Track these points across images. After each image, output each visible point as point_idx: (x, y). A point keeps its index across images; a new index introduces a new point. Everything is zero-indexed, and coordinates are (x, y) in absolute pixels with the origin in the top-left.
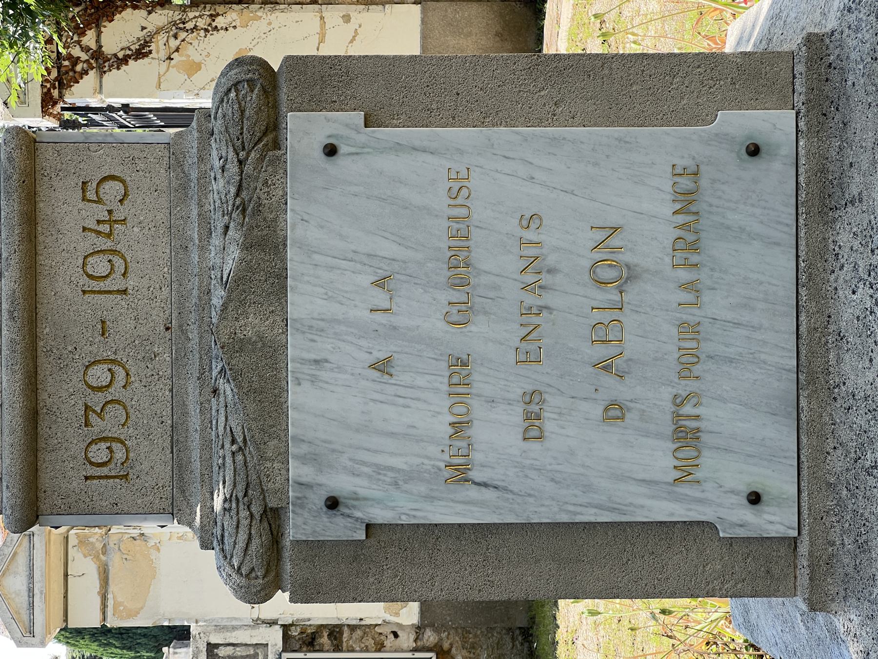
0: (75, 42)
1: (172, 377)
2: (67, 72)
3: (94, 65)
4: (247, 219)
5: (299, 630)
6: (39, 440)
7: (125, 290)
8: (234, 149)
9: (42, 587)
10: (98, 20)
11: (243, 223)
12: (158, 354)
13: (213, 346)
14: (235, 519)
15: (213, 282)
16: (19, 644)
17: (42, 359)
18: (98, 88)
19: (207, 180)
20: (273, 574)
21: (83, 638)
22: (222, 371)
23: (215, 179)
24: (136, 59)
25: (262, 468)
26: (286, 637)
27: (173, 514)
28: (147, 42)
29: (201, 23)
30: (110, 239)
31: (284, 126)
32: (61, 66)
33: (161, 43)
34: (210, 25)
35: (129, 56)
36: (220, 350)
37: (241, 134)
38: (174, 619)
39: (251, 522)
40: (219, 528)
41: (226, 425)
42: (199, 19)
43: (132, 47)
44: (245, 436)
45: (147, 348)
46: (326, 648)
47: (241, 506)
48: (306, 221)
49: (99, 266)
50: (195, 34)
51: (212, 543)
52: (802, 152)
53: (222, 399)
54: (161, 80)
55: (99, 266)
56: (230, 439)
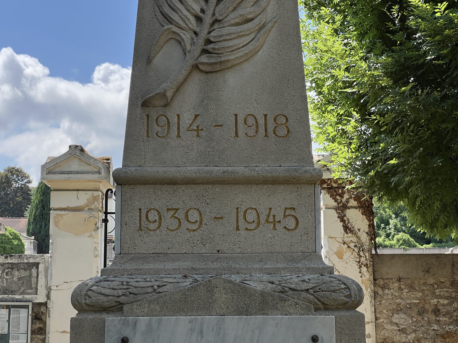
0: (351, 196)
1: (193, 254)
2: (335, 191)
3: (340, 205)
4: (277, 294)
5: (44, 311)
6: (160, 185)
7: (238, 229)
8: (314, 287)
9: (72, 178)
10: (362, 207)
11: (275, 292)
12: (205, 246)
13: (209, 275)
14: (117, 287)
15: (243, 276)
16: (43, 167)
17: (202, 187)
18: (328, 207)
19: (297, 272)
20: (87, 308)
21: (41, 196)
22: (196, 281)
23: (298, 277)
24: (343, 226)
25: (145, 302)
26: (40, 304)
27: (120, 254)
28: (352, 232)
29: (363, 259)
30: (265, 222)
31: (327, 314)
32: (339, 189)
33: (352, 239)
34: (362, 264)
35: (345, 223)
36: (208, 280)
37: (322, 291)
38: (53, 245)
39: (116, 296)
40: (112, 279)
41: (168, 282)
42: (365, 259)
43: (349, 224)
44: (162, 293)
45: (208, 241)
46: (34, 326)
47: (124, 291)
48: (277, 326)
49: (251, 216)
50: (357, 256)
51: (104, 275)
53: (182, 280)
54: (333, 239)
55: (251, 216)
56: (160, 285)
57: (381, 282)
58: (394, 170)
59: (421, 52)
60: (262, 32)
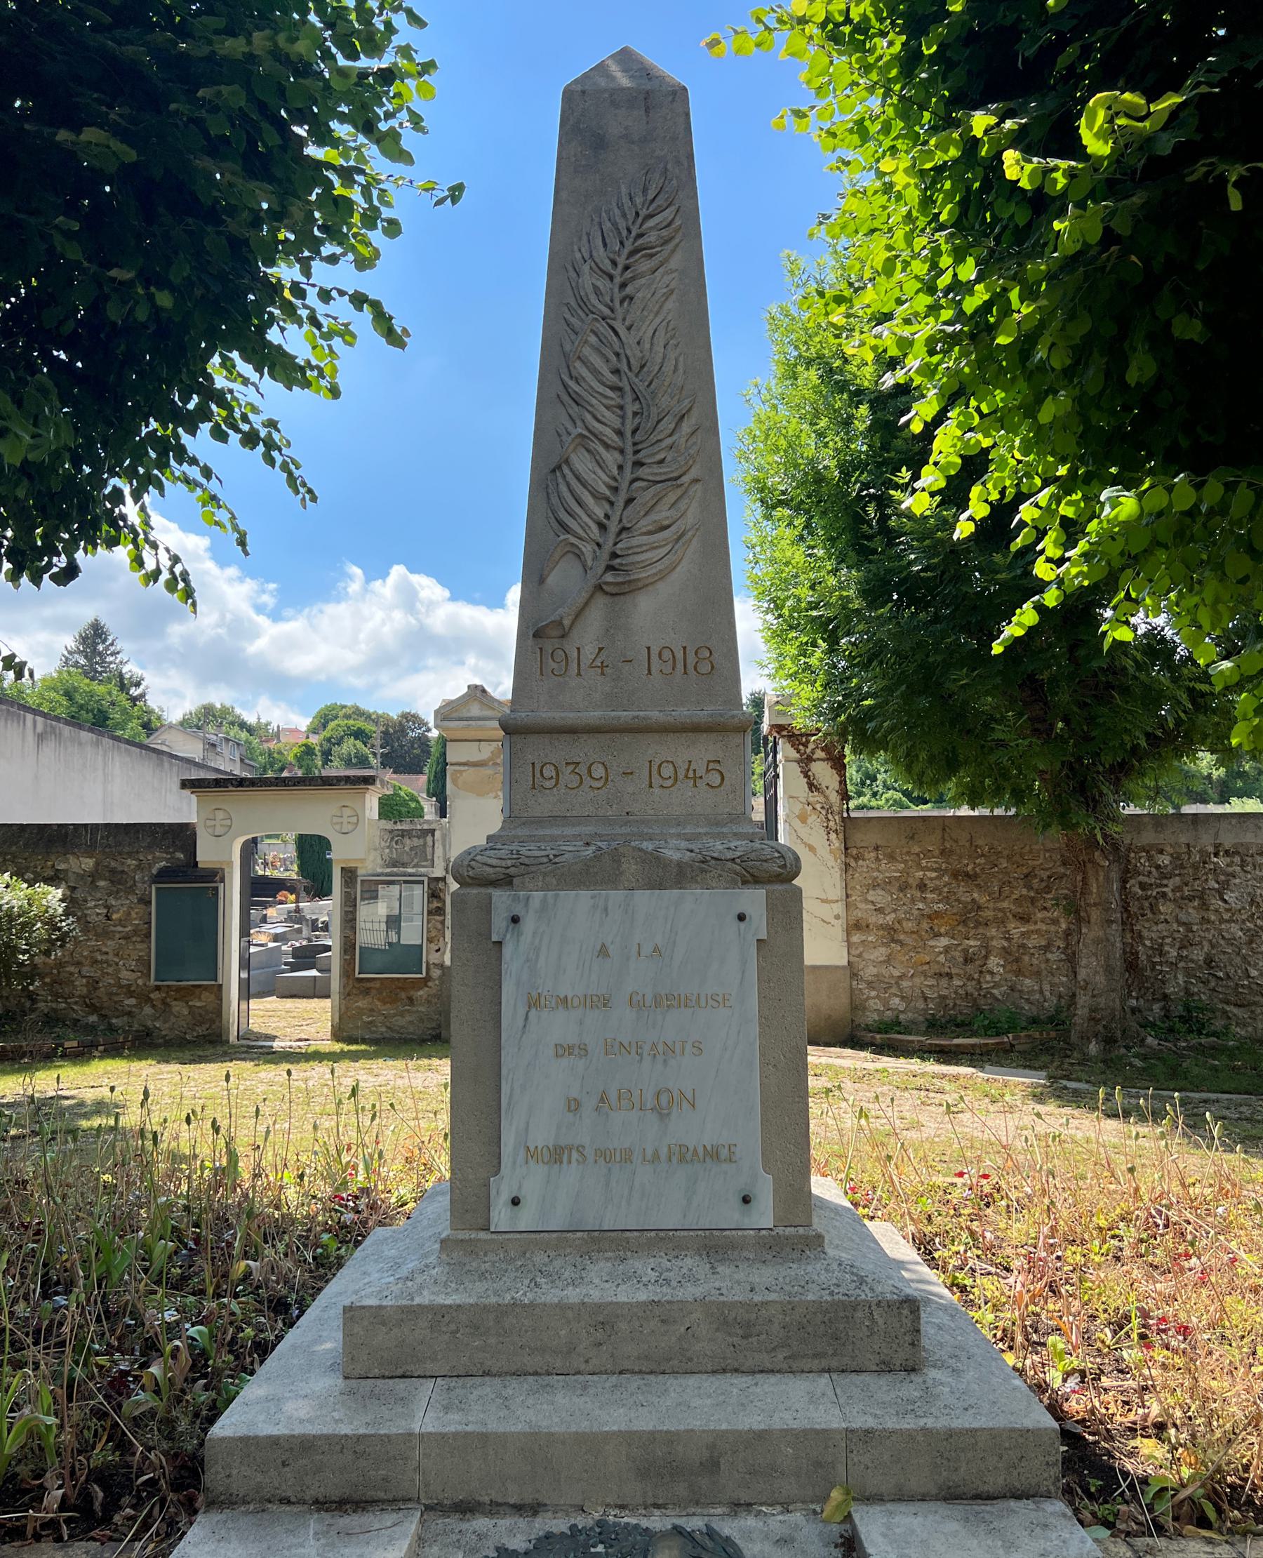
17: (608, 736)
22: (600, 849)
26: (437, 879)
29: (832, 824)
49: (667, 771)
52: (746, 1233)
55: (667, 771)
57: (855, 852)
58: (869, 714)
59: (905, 562)
60: (681, 542)
